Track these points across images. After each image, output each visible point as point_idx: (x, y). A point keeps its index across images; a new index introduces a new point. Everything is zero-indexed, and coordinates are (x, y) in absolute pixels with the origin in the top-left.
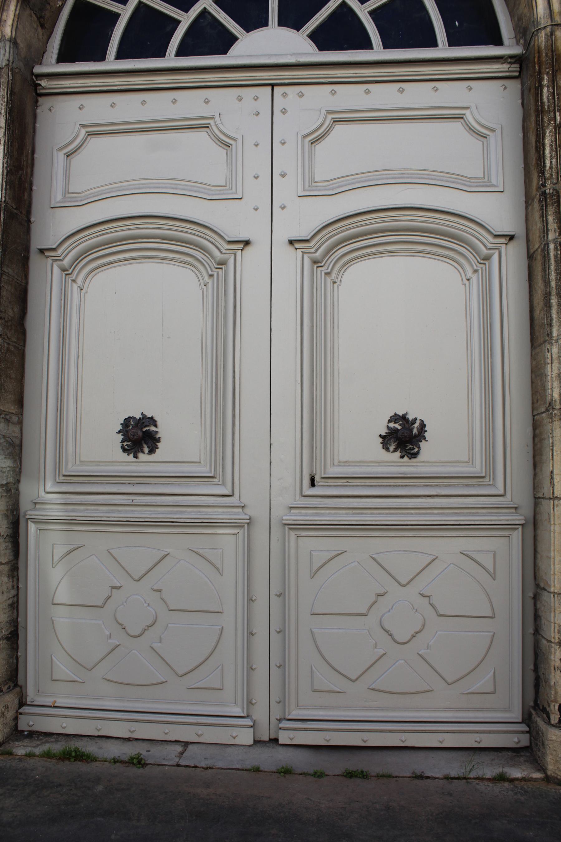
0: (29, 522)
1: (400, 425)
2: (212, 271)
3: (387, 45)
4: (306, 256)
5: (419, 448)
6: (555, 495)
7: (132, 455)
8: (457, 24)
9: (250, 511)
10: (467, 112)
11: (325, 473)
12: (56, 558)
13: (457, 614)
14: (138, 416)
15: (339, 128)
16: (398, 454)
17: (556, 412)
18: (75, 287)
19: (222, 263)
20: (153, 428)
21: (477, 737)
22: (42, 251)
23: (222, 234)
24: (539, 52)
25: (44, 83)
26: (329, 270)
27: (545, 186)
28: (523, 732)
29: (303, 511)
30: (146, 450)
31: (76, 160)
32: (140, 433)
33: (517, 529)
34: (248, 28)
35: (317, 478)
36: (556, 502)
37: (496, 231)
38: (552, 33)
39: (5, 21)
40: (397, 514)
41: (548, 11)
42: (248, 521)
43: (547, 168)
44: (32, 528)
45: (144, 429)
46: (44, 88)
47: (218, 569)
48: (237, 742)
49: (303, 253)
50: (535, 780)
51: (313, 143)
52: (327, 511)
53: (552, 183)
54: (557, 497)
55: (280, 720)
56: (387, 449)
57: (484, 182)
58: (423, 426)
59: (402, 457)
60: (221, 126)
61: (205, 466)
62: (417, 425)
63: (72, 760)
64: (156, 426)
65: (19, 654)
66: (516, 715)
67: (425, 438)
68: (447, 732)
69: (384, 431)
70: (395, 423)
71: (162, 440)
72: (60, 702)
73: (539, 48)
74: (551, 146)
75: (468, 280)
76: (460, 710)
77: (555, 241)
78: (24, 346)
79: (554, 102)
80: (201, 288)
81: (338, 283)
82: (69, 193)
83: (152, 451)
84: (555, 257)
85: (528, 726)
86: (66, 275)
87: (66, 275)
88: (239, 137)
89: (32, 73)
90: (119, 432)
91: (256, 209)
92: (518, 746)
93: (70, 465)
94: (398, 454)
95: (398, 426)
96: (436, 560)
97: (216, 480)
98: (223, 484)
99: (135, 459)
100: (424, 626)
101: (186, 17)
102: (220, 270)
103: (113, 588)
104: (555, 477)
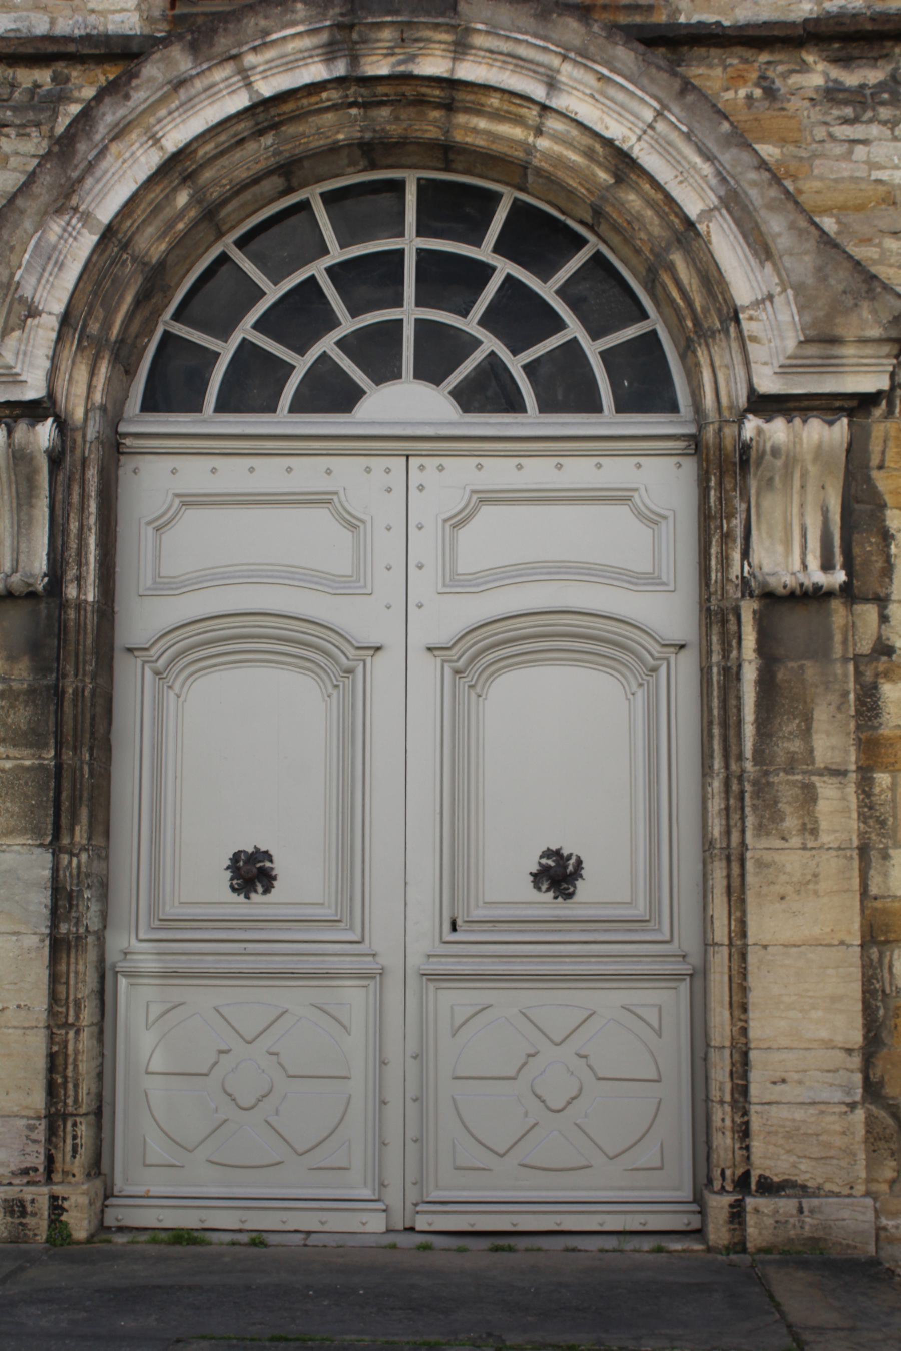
0: (119, 976)
1: (554, 861)
2: (337, 680)
3: (546, 406)
4: (446, 666)
5: (575, 887)
6: (715, 941)
7: (242, 896)
8: (626, 384)
9: (382, 960)
10: (636, 495)
11: (468, 916)
12: (152, 1018)
13: (618, 1076)
14: (250, 850)
15: (485, 510)
16: (551, 894)
17: (716, 851)
18: (172, 694)
19: (350, 671)
20: (268, 864)
21: (642, 1218)
22: (130, 650)
23: (349, 638)
24: (707, 448)
25: (128, 442)
26: (473, 683)
27: (710, 602)
28: (693, 1212)
29: (443, 960)
30: (260, 889)
31: (168, 537)
32: (255, 870)
33: (684, 980)
34: (379, 380)
35: (459, 922)
36: (716, 948)
37: (663, 640)
38: (720, 430)
39: (95, 387)
40: (548, 962)
41: (716, 405)
42: (380, 971)
43: (713, 581)
44: (123, 982)
45: (259, 865)
46: (128, 447)
47: (344, 1027)
48: (368, 1229)
49: (443, 662)
50: (697, 1251)
51: (454, 527)
52: (471, 960)
53: (717, 599)
54: (717, 944)
55: (416, 1205)
56: (539, 889)
57: (653, 579)
58: (579, 862)
59: (556, 898)
60: (346, 504)
61: (329, 907)
62: (573, 861)
63: (185, 1243)
64: (271, 861)
65: (103, 1136)
66: (686, 1193)
67: (581, 876)
68: (609, 1213)
69: (535, 868)
70: (548, 858)
71: (279, 878)
72: (155, 1191)
73: (707, 444)
74: (717, 557)
75: (633, 694)
76: (621, 1189)
77: (718, 664)
78: (110, 765)
79: (721, 508)
80: (324, 700)
81: (484, 696)
82: (160, 577)
83: (267, 891)
84: (718, 682)
85: (700, 1206)
86: (160, 679)
87: (160, 679)
88: (367, 518)
89: (116, 432)
90: (228, 868)
91: (389, 608)
92: (689, 1228)
93: (167, 908)
94: (551, 894)
95: (551, 863)
96: (594, 1016)
97: (342, 925)
98: (351, 928)
99: (246, 901)
100: (581, 1090)
101: (302, 363)
102: (346, 679)
103: (221, 1052)
104: (715, 921)
